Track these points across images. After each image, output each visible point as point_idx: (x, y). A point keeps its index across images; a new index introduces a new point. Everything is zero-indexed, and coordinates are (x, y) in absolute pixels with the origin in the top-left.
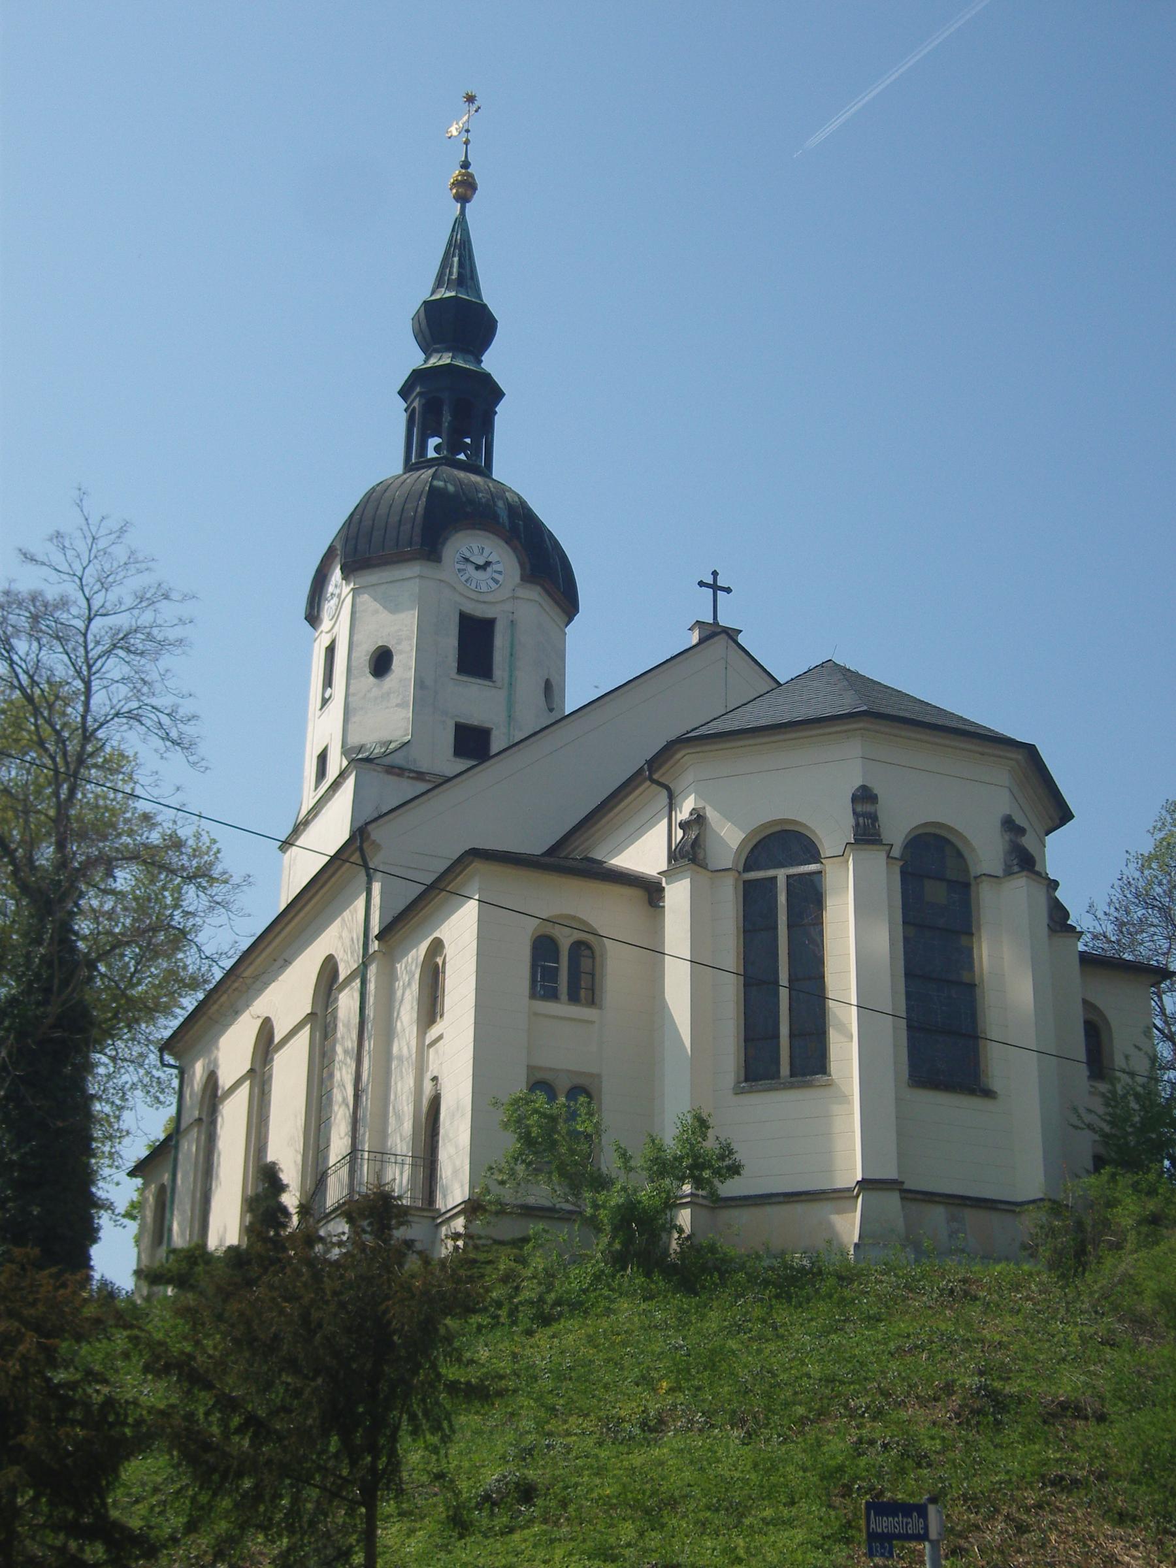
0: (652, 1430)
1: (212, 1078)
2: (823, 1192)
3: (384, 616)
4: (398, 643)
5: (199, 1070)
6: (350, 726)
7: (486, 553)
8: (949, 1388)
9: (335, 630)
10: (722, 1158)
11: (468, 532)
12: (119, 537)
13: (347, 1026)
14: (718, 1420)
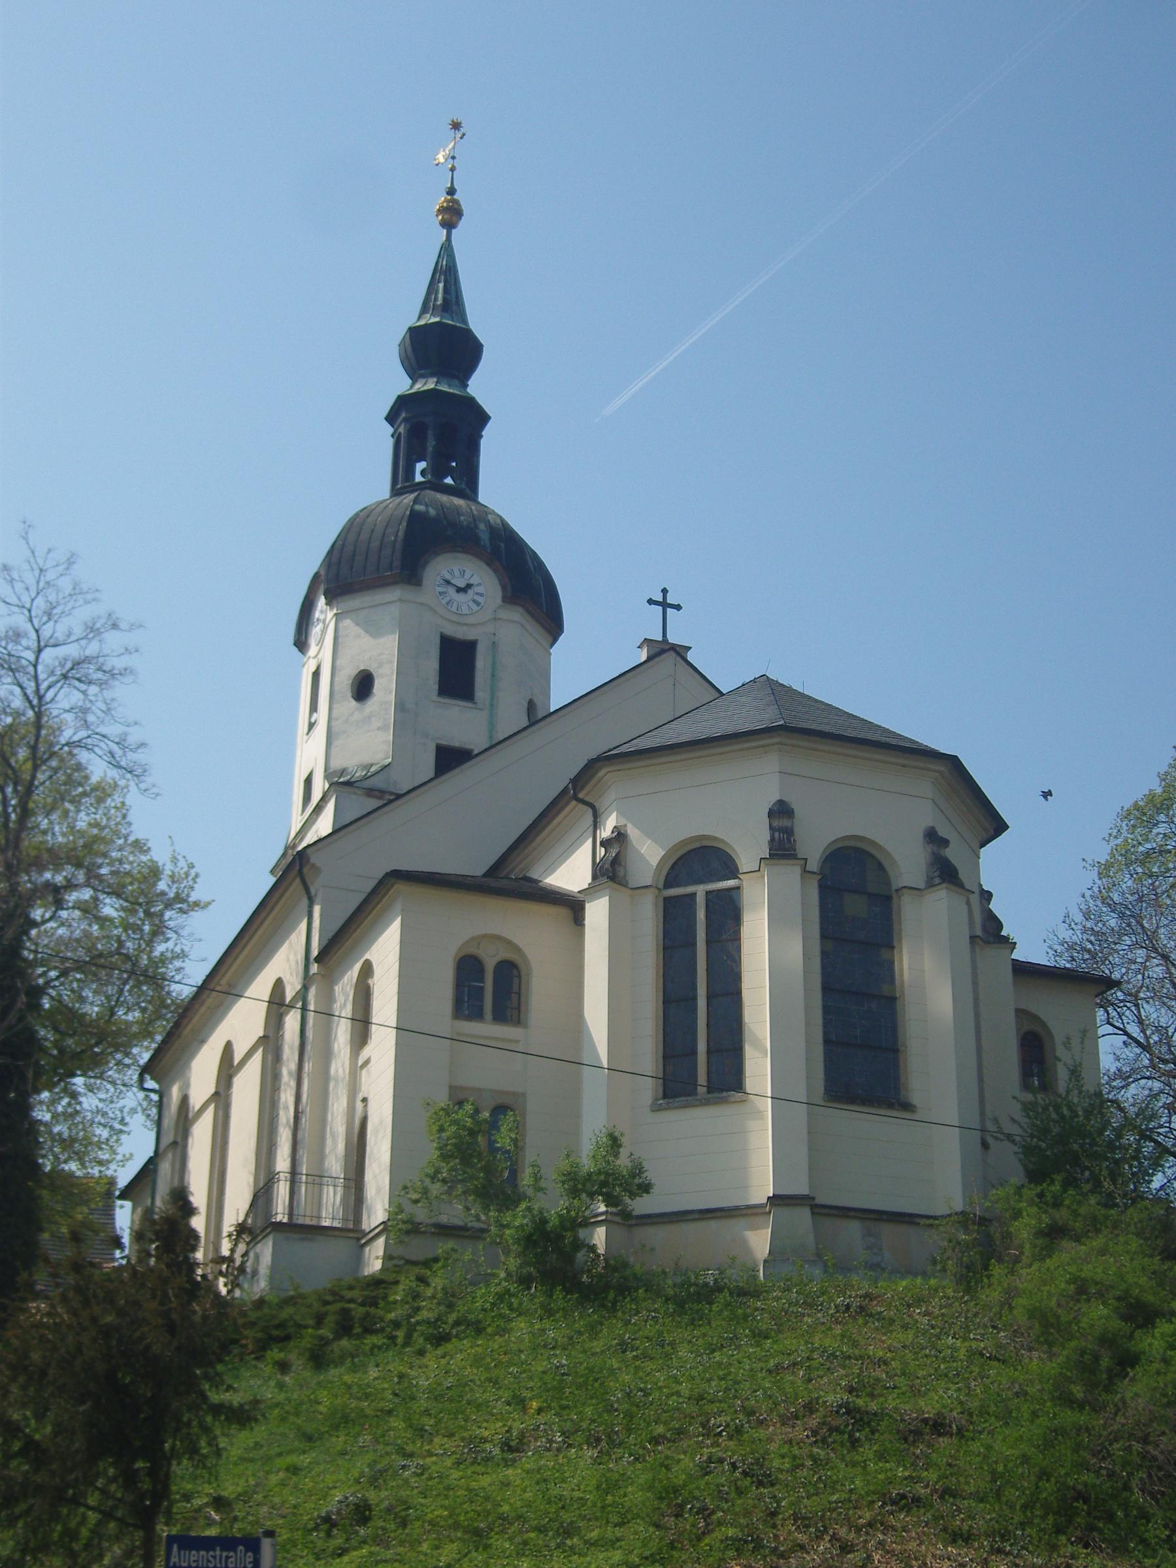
0: (511, 1449)
1: (185, 1100)
2: (737, 1208)
3: (366, 641)
4: (380, 666)
5: (175, 1092)
6: (333, 751)
7: (467, 576)
8: (810, 1408)
9: (320, 656)
10: (633, 1175)
11: (449, 555)
12: (67, 569)
13: (291, 1048)
14: (579, 1438)
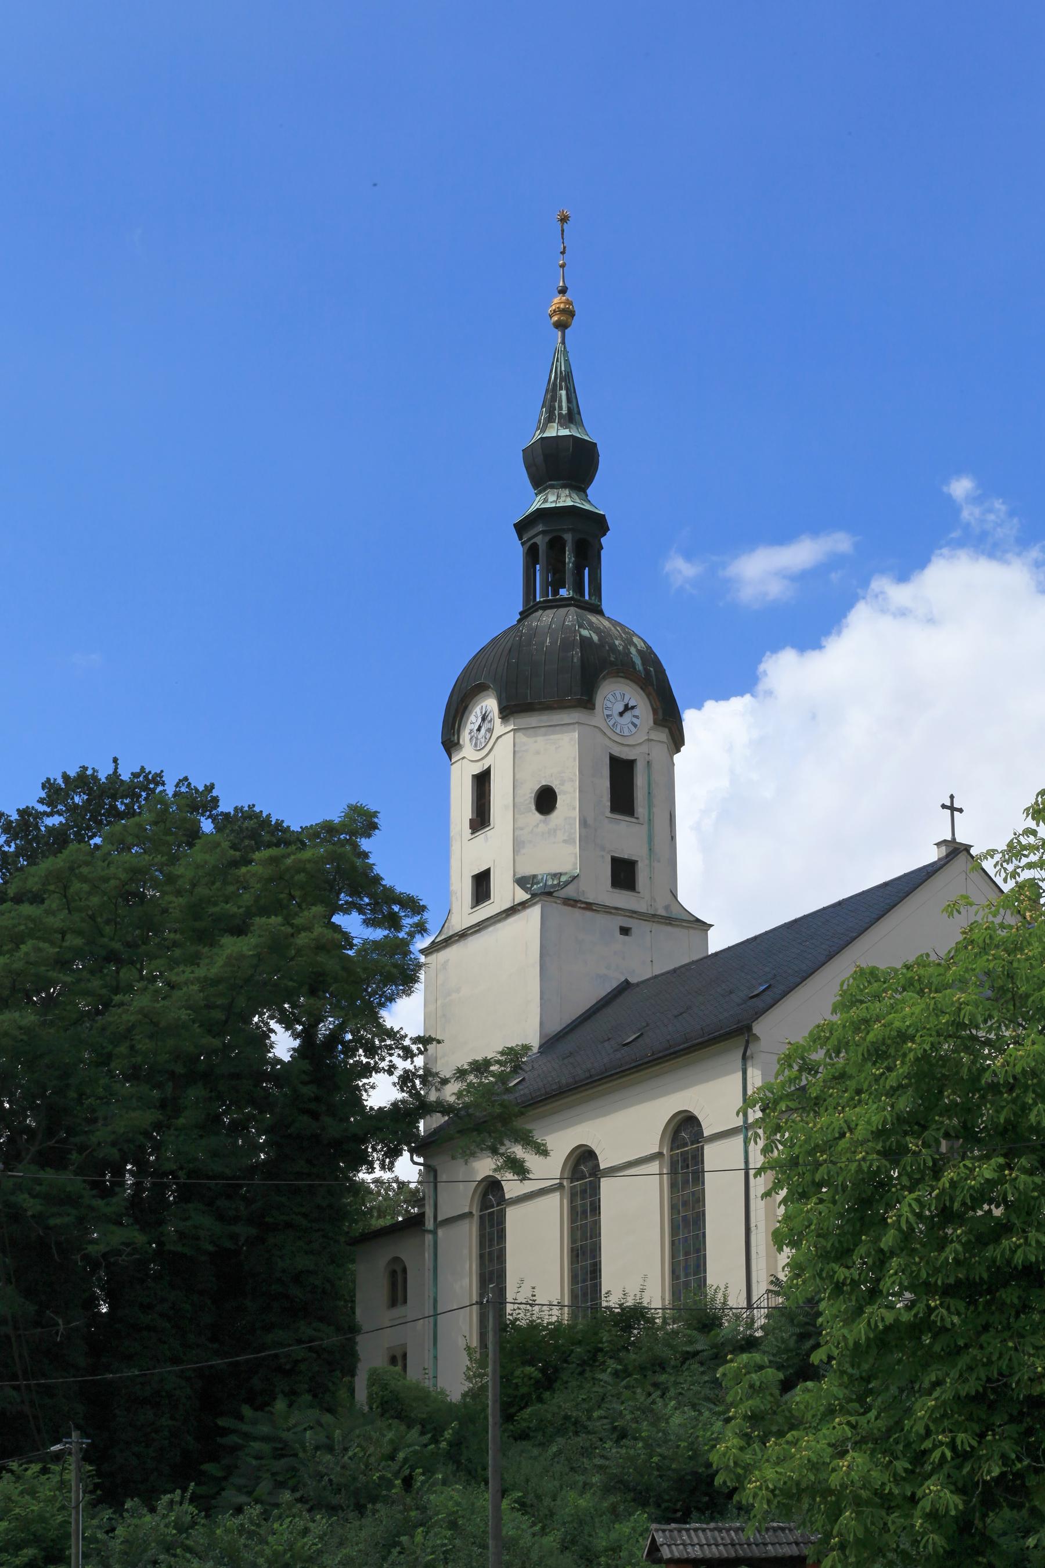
4: (562, 783)
